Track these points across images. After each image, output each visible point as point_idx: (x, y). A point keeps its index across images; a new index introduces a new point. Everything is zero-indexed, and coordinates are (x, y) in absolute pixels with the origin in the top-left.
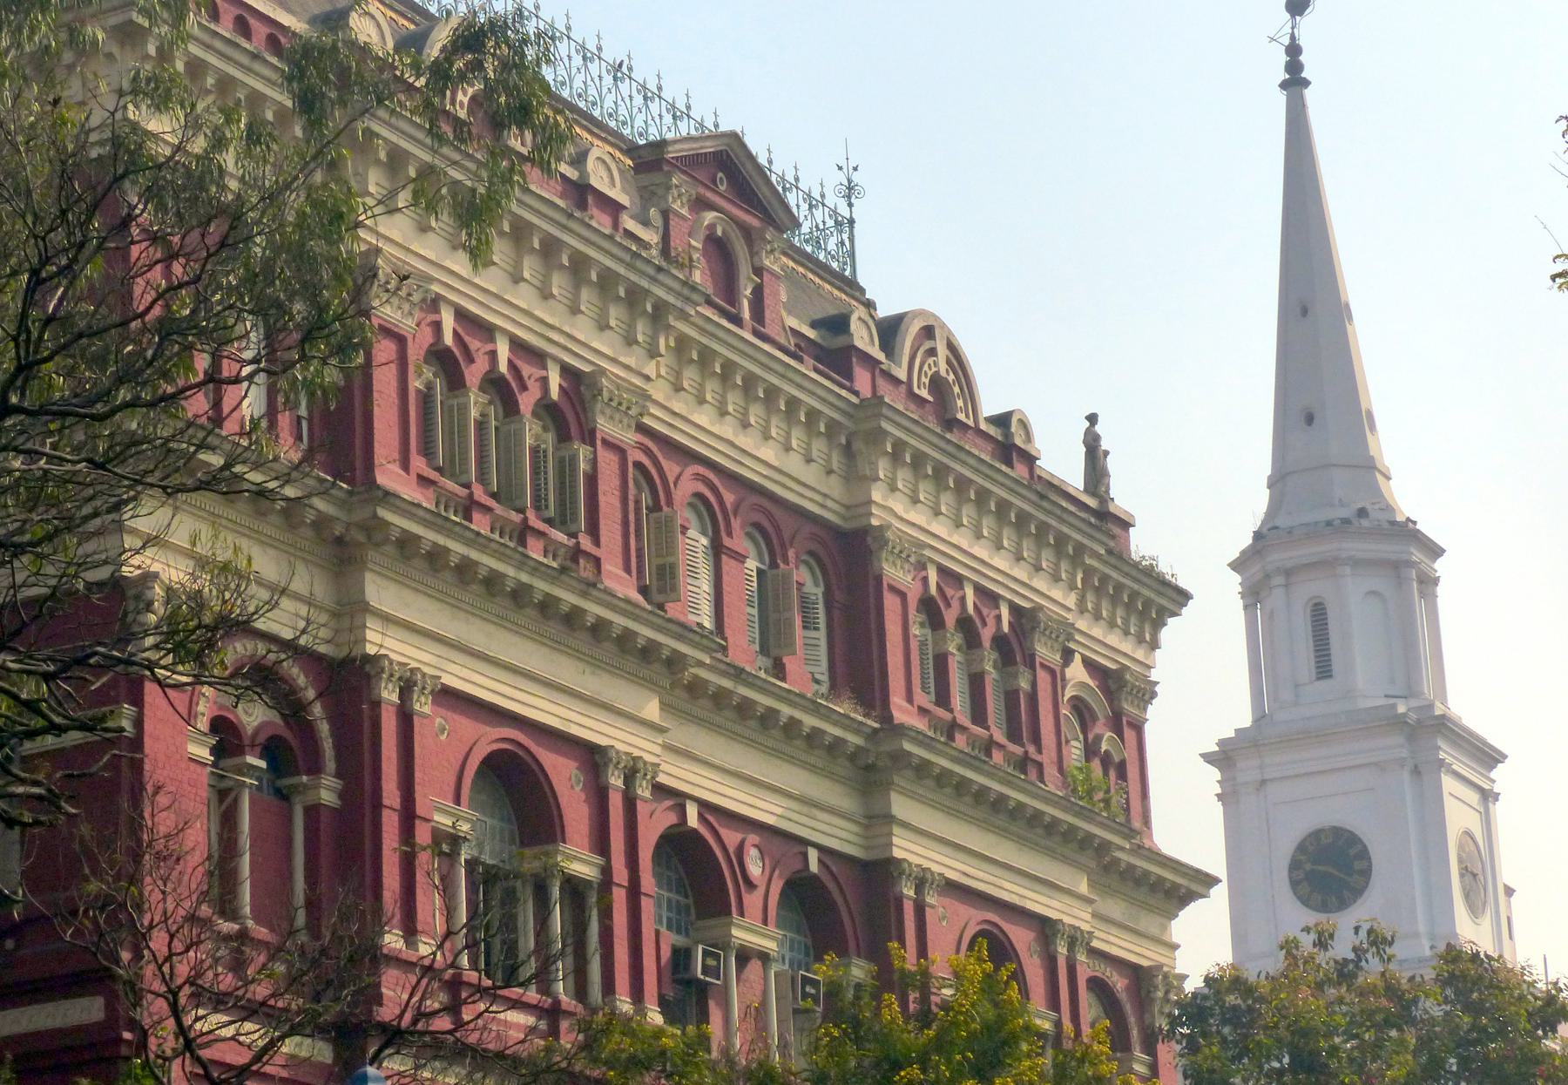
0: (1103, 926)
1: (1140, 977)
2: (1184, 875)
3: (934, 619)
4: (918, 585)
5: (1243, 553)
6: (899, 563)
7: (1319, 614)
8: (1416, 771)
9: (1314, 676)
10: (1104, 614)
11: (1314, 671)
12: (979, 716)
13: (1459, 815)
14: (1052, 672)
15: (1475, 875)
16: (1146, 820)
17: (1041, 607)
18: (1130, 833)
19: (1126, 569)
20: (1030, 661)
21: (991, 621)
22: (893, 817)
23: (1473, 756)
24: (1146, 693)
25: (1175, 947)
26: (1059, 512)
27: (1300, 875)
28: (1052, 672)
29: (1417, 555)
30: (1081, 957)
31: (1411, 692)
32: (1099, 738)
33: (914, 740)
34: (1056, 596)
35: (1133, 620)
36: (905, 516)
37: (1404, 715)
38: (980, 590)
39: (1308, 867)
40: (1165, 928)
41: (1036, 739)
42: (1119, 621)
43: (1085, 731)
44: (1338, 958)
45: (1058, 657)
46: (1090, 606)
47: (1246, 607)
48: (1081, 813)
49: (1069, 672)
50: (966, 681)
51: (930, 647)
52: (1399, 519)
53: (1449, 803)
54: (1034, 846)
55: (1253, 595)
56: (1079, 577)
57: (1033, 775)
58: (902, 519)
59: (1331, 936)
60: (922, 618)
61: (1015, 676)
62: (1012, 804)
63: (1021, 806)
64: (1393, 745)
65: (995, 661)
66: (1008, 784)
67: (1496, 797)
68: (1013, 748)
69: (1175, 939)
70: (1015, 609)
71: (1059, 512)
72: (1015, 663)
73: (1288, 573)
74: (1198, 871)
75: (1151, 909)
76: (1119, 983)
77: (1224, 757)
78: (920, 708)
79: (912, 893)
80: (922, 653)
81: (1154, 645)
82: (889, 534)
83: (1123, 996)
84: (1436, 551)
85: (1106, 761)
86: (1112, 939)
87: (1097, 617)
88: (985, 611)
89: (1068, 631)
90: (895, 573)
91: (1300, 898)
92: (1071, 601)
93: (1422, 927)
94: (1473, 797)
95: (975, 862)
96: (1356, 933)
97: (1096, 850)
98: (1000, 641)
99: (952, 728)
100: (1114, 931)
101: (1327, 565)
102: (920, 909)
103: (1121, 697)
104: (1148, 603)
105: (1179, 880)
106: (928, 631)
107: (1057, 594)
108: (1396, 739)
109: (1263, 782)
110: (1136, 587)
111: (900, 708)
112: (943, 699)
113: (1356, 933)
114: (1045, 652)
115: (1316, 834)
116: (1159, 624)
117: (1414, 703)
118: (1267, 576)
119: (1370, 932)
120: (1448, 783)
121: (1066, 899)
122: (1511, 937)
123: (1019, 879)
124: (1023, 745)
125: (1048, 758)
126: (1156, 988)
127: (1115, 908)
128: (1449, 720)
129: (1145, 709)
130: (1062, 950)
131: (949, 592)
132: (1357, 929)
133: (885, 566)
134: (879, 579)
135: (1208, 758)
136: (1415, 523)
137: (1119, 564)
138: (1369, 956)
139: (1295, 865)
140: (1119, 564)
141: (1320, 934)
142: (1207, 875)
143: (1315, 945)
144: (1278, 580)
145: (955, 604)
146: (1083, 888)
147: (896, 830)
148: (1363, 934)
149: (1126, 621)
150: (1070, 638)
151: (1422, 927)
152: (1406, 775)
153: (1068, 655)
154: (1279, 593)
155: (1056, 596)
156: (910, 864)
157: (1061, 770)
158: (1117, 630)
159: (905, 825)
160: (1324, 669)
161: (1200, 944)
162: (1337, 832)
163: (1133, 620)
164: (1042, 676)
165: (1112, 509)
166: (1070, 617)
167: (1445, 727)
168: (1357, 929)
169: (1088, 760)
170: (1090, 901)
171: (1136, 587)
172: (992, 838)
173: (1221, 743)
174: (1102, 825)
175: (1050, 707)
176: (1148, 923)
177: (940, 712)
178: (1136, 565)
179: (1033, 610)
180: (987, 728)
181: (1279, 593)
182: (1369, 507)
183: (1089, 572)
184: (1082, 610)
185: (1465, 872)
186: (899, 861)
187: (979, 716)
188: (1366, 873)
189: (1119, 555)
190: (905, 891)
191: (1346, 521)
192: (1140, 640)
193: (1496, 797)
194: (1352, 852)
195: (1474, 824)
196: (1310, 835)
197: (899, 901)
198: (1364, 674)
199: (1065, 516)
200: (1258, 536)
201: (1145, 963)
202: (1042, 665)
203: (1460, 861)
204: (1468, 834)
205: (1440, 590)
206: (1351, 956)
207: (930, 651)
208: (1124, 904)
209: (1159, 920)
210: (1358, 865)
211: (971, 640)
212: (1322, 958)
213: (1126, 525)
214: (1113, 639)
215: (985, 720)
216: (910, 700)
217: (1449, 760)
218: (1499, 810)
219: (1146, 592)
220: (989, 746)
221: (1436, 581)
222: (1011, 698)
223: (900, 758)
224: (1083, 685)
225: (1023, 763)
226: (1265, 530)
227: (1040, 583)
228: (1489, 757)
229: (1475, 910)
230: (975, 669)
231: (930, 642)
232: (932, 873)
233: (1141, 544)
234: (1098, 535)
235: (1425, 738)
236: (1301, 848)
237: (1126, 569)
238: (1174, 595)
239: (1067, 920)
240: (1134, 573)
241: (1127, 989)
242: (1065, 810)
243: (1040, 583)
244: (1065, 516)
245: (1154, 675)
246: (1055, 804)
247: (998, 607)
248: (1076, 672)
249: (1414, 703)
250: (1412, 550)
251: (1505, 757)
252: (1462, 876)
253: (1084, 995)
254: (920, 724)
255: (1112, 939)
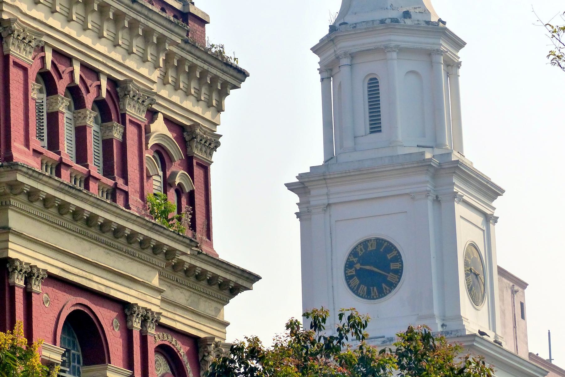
0: (171, 309)
1: (197, 344)
2: (233, 273)
3: (50, 88)
4: (38, 62)
5: (322, 41)
6: (22, 46)
7: (373, 86)
8: (437, 200)
9: (368, 130)
10: (181, 86)
11: (368, 127)
12: (81, 157)
13: (467, 232)
14: (139, 126)
15: (477, 275)
16: (209, 234)
17: (131, 80)
18: (192, 243)
19: (199, 54)
20: (122, 119)
21: (93, 90)
22: (10, 229)
23: (479, 190)
24: (213, 143)
25: (226, 324)
26: (146, 12)
27: (352, 272)
28: (139, 126)
29: (445, 46)
30: (151, 330)
31: (437, 143)
32: (174, 174)
33: (25, 174)
34: (144, 72)
35: (204, 90)
36: (28, 13)
37: (430, 160)
38: (84, 67)
39: (358, 266)
40: (218, 311)
41: (124, 175)
42: (193, 91)
43: (164, 170)
44: (327, 336)
45: (143, 116)
46: (170, 79)
47: (322, 80)
48: (153, 228)
49: (153, 127)
50: (73, 133)
51: (45, 107)
52: (434, 19)
53: (460, 225)
54: (119, 251)
55: (327, 72)
56: (162, 58)
57: (120, 199)
58: (26, 15)
59: (324, 320)
60: (41, 85)
61: (111, 129)
62: (101, 221)
63: (107, 222)
64: (422, 181)
65: (96, 118)
66: (98, 206)
67: (496, 219)
68: (105, 180)
69: (226, 319)
70: (112, 82)
71: (146, 12)
72: (110, 120)
73: (352, 56)
74: (243, 271)
75: (209, 297)
76: (182, 350)
77: (302, 186)
78: (34, 151)
79: (22, 283)
80: (40, 112)
81: (220, 109)
82: (15, 26)
83: (185, 359)
84: (459, 44)
85: (179, 191)
86: (177, 318)
87: (176, 88)
88: (89, 82)
89: (151, 96)
90: (18, 53)
91: (352, 289)
92: (155, 75)
93: (436, 312)
94: (479, 220)
95: (72, 261)
96: (341, 318)
97: (166, 254)
98: (100, 105)
99: (59, 166)
100: (179, 312)
101: (382, 50)
102: (28, 295)
103: (193, 146)
104: (215, 79)
105: (228, 277)
106: (44, 96)
107: (144, 71)
108: (424, 177)
109: (329, 205)
110: (206, 67)
111: (19, 151)
112: (53, 145)
113: (341, 318)
114: (134, 112)
115: (365, 243)
116: (223, 93)
117: (438, 152)
118: (338, 58)
119: (349, 318)
120: (460, 209)
121: (144, 290)
122: (523, 317)
123: (104, 274)
124: (114, 179)
125: (133, 188)
126: (209, 353)
127: (180, 296)
128: (462, 164)
129: (211, 155)
130: (137, 325)
131: (61, 68)
132: (341, 316)
133: (12, 48)
134: (6, 58)
135: (290, 187)
136: (444, 23)
137: (193, 51)
138: (349, 335)
139: (349, 265)
140: (193, 51)
141: (316, 318)
142: (250, 274)
143: (311, 328)
144: (345, 61)
145: (66, 76)
146: (155, 281)
147: (11, 238)
148: (345, 320)
149: (198, 91)
150: (153, 102)
151: (436, 312)
152: (429, 203)
153: (152, 114)
154: (345, 71)
155: (144, 72)
156: (21, 263)
157: (142, 197)
158: (192, 98)
159: (19, 235)
160: (375, 126)
161: (259, 318)
162: (380, 242)
163: (204, 90)
164: (131, 131)
165: (192, 10)
166: (155, 88)
167: (458, 169)
168: (341, 316)
169: (165, 192)
170: (160, 291)
171: (206, 67)
172: (86, 245)
173: (300, 176)
174: (168, 237)
175: (136, 152)
176: (206, 307)
177: (52, 155)
178: (206, 52)
179: (125, 82)
180: (87, 166)
181: (345, 71)
182: (412, 11)
183: (169, 56)
184: (165, 83)
185: (469, 272)
186: (13, 261)
187: (81, 157)
188: (399, 272)
189: (194, 44)
190: (17, 282)
191: (395, 21)
192: (209, 105)
193: (496, 219)
194: (389, 256)
195: (479, 239)
196: (360, 244)
197: (12, 288)
198: (403, 129)
199: (150, 15)
200: (332, 28)
201: (202, 335)
202: (131, 121)
203: (466, 264)
204: (474, 245)
205: (461, 71)
206: (337, 335)
207: (45, 111)
208: (187, 294)
209: (215, 305)
210: (393, 266)
211: (78, 102)
212: (315, 335)
213: (203, 22)
214: (188, 104)
215: (86, 160)
216: (27, 144)
217: (460, 192)
218: (497, 229)
219: (214, 71)
220: (87, 179)
221: (458, 65)
222: (107, 144)
223: (15, 186)
224: (164, 136)
225: (113, 193)
226: (337, 25)
227: (131, 63)
228: (492, 191)
229: (476, 300)
230: (80, 123)
231: (45, 104)
232: (38, 269)
233: (214, 36)
234: (176, 30)
235: (444, 176)
236: (354, 253)
237: (199, 54)
238: (235, 73)
239: (141, 304)
240: (205, 57)
241: (188, 353)
242: (143, 226)
243: (131, 63)
244: (150, 15)
245: (219, 130)
246: (134, 222)
247: (99, 79)
248: (159, 127)
249: (438, 152)
250: (442, 42)
251: (503, 191)
252: (467, 275)
253: (152, 356)
254: (34, 163)
255: (177, 318)
